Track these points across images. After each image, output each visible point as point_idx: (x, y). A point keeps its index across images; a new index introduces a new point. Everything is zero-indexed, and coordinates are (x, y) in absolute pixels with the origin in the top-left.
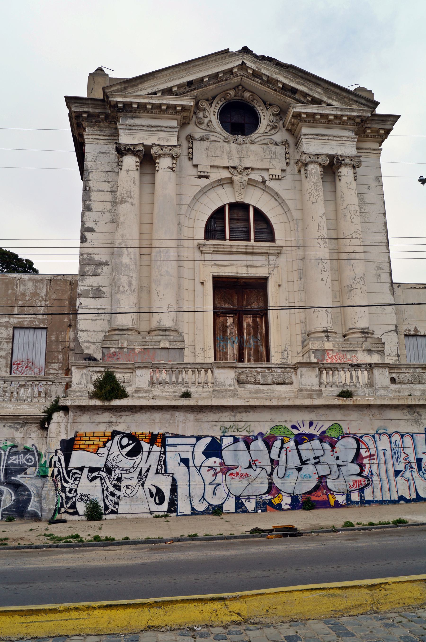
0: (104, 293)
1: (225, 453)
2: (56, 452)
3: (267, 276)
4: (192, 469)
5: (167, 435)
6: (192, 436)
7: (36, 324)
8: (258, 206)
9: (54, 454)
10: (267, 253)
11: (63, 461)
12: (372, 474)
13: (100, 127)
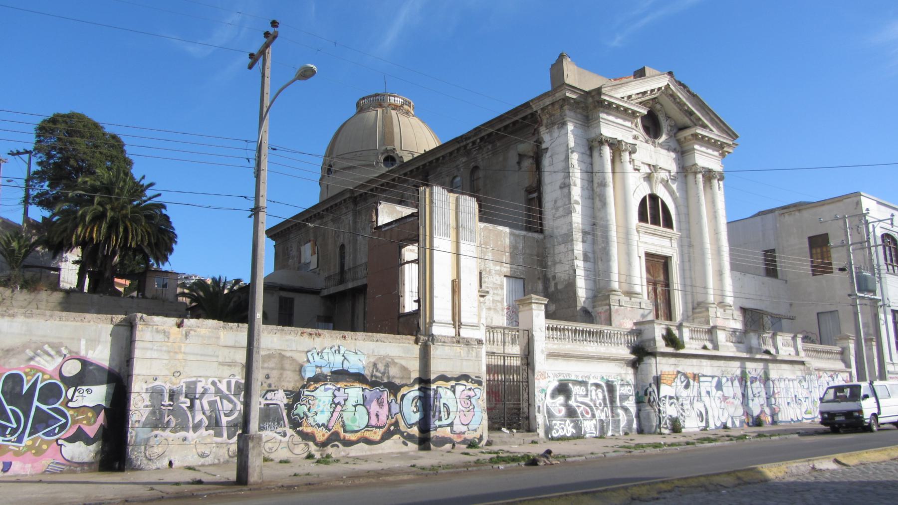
2: (650, 385)
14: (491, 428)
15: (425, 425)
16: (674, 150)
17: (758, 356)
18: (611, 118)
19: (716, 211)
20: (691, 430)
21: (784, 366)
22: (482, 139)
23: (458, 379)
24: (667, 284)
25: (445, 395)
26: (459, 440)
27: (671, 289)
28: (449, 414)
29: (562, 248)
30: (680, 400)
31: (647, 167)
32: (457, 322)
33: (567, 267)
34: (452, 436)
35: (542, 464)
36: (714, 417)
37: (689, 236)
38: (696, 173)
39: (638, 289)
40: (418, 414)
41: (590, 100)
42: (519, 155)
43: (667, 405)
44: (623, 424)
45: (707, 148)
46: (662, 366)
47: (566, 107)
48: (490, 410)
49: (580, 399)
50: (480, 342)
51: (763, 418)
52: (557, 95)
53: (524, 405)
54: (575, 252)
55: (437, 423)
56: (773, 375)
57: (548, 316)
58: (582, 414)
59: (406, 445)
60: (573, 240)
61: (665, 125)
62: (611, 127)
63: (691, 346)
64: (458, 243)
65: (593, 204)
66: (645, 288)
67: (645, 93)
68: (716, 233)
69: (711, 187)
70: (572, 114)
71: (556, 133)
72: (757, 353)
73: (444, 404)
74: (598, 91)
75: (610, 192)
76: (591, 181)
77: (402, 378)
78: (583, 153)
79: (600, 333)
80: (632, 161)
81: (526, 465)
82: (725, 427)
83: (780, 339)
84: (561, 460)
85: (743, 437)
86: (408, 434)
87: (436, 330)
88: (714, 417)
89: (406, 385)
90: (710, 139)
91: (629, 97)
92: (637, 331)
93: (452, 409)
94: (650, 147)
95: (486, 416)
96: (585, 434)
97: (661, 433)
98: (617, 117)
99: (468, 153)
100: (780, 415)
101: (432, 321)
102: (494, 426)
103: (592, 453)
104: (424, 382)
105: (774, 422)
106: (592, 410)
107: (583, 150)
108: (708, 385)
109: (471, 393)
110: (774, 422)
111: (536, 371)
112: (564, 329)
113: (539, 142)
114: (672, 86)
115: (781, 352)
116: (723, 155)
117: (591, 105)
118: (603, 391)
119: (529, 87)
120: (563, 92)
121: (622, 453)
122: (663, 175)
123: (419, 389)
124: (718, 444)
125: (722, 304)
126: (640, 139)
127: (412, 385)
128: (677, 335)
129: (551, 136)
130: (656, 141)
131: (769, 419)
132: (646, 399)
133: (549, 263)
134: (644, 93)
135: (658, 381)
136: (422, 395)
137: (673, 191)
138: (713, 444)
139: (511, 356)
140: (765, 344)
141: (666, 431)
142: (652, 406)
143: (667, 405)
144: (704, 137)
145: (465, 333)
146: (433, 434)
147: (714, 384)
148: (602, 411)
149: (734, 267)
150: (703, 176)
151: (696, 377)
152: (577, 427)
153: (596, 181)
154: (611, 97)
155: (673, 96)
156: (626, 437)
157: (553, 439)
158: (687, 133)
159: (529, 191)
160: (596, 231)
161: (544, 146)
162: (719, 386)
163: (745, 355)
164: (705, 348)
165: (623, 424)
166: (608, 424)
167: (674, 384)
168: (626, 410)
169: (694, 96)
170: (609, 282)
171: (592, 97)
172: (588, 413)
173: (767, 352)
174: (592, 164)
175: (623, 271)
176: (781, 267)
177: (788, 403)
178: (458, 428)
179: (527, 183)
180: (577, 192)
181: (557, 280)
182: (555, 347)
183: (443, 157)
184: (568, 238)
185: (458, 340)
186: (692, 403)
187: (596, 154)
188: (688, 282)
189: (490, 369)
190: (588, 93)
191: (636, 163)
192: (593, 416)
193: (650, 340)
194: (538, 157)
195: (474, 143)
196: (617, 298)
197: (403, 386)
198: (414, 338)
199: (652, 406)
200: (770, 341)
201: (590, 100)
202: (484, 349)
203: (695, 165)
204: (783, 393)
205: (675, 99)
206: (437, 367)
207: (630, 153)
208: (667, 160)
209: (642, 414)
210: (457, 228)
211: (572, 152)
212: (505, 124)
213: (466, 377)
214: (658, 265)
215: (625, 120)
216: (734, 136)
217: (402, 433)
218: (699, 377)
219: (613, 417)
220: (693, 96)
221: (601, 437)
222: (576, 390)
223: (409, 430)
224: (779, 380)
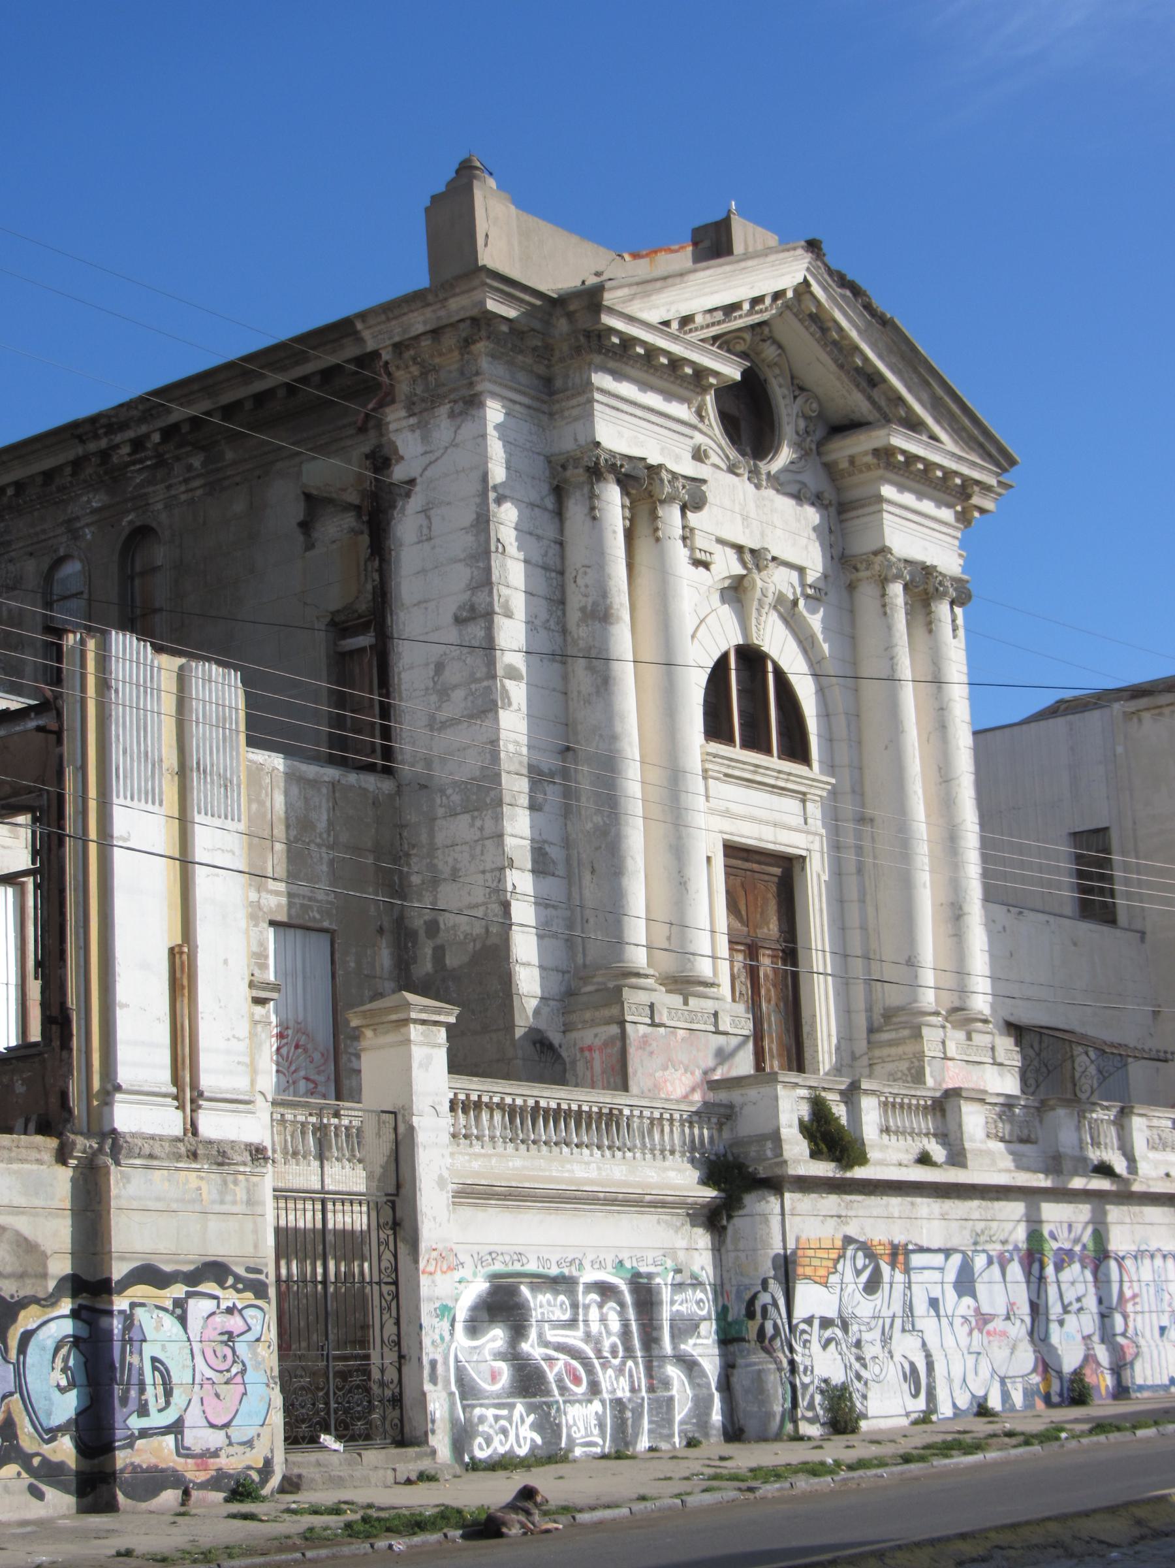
0: (553, 862)
1: (980, 1288)
2: (765, 1284)
3: (804, 853)
4: (944, 1321)
5: (910, 1247)
6: (939, 1250)
7: (314, 918)
8: (785, 666)
9: (760, 1288)
10: (804, 794)
11: (782, 1302)
12: (1137, 1334)
13: (511, 363)
14: (293, 1439)
15: (95, 1431)
16: (817, 501)
17: (1077, 1183)
18: (627, 389)
19: (939, 709)
20: (884, 1424)
21: (1153, 1213)
22: (169, 433)
23: (193, 1278)
24: (791, 951)
25: (157, 1334)
26: (202, 1477)
27: (801, 969)
28: (168, 1393)
29: (461, 828)
30: (854, 1328)
31: (731, 554)
32: (186, 1089)
33: (479, 895)
34: (179, 1463)
35: (515, 1531)
36: (950, 1379)
37: (858, 790)
38: (883, 582)
39: (704, 968)
40: (73, 1394)
41: (562, 325)
42: (308, 497)
43: (815, 1346)
44: (681, 1411)
45: (920, 495)
46: (801, 1221)
47: (481, 347)
48: (287, 1380)
49: (553, 1336)
50: (258, 1154)
51: (1090, 1378)
52: (454, 304)
53: (380, 1358)
54: (509, 842)
55: (136, 1423)
56: (1119, 1241)
57: (455, 1067)
58: (559, 1381)
59: (38, 1495)
60: (499, 802)
61: (789, 414)
62: (629, 422)
63: (888, 1155)
64: (184, 823)
65: (565, 678)
66: (724, 967)
67: (735, 306)
68: (944, 777)
69: (930, 626)
70: (500, 370)
71: (443, 428)
72: (1075, 1173)
73: (154, 1360)
74: (591, 299)
75: (622, 640)
76: (558, 601)
77: (22, 1276)
78: (532, 505)
79: (610, 1119)
80: (687, 537)
81: (463, 1537)
82: (983, 1411)
83: (1139, 1126)
84: (562, 1518)
85: (1049, 1436)
86: (45, 1461)
87: (127, 1117)
88: (950, 1379)
89: (35, 1300)
90: (930, 466)
91: (686, 320)
92: (720, 1108)
93: (180, 1375)
94: (742, 486)
95: (278, 1400)
96: (570, 1449)
97: (798, 1438)
98: (645, 386)
99: (111, 474)
100: (1138, 1366)
101: (111, 1087)
102: (299, 1435)
103: (643, 1498)
104: (90, 1290)
105: (1121, 1391)
106: (590, 1370)
107: (534, 496)
108: (932, 1277)
109: (235, 1323)
110: (1121, 1391)
111: (423, 1246)
112: (478, 1105)
113: (381, 460)
114: (816, 289)
115: (1143, 1167)
116: (964, 518)
117: (565, 342)
118: (622, 1304)
119: (361, 271)
120: (477, 295)
121: (733, 1494)
122: (781, 581)
123: (75, 1314)
124: (992, 1455)
125: (959, 1015)
126: (714, 459)
127: (51, 1301)
128: (844, 1121)
129: (425, 439)
130: (763, 466)
131: (1107, 1381)
132: (752, 1328)
133: (415, 880)
134: (731, 309)
135: (787, 1270)
136: (84, 1333)
137: (812, 637)
138: (978, 1457)
139: (348, 1198)
140: (1096, 1143)
141: (814, 1431)
142: (769, 1351)
143: (815, 1346)
144: (912, 458)
145: (215, 1125)
146: (122, 1458)
147: (951, 1275)
148: (620, 1371)
149: (990, 896)
150: (906, 587)
151: (899, 1254)
152: (548, 1425)
153: (575, 601)
154: (631, 319)
155: (819, 322)
156: (692, 1452)
157: (475, 1466)
158: (860, 444)
159: (341, 626)
160: (576, 769)
161: (399, 473)
162: (965, 1283)
163: (1041, 1181)
164: (924, 1159)
165: (681, 1411)
166: (638, 1416)
167: (834, 1279)
168: (690, 1365)
169: (884, 322)
170: (617, 942)
171: (570, 316)
172: (577, 1380)
173: (1104, 1170)
174: (561, 544)
175: (661, 914)
176: (1128, 896)
177: (1163, 1329)
178: (198, 1437)
179: (334, 599)
180: (512, 635)
181: (443, 937)
182: (476, 1165)
183: (20, 486)
184: (484, 797)
185: (193, 1148)
186: (886, 1339)
187: (575, 509)
188: (856, 948)
189: (289, 1242)
190: (556, 304)
191: (700, 541)
192: (594, 1388)
193: (761, 1139)
194: (376, 512)
195: (138, 444)
196: (643, 997)
197: (23, 1303)
198: (52, 1143)
199: (769, 1351)
200: (1110, 1134)
201: (562, 325)
202: (268, 1180)
203: (884, 550)
204: (1148, 1298)
205: (824, 330)
206: (133, 1237)
207: (684, 509)
208: (792, 533)
209: (740, 1379)
210: (183, 772)
211: (499, 501)
212: (258, 386)
213: (216, 1271)
214: (764, 881)
215: (669, 396)
216: (1002, 459)
217: (24, 1459)
218: (907, 1253)
219: (651, 1389)
220: (881, 323)
221: (619, 1456)
222: (543, 1306)
223: (46, 1449)
224: (1137, 1256)
